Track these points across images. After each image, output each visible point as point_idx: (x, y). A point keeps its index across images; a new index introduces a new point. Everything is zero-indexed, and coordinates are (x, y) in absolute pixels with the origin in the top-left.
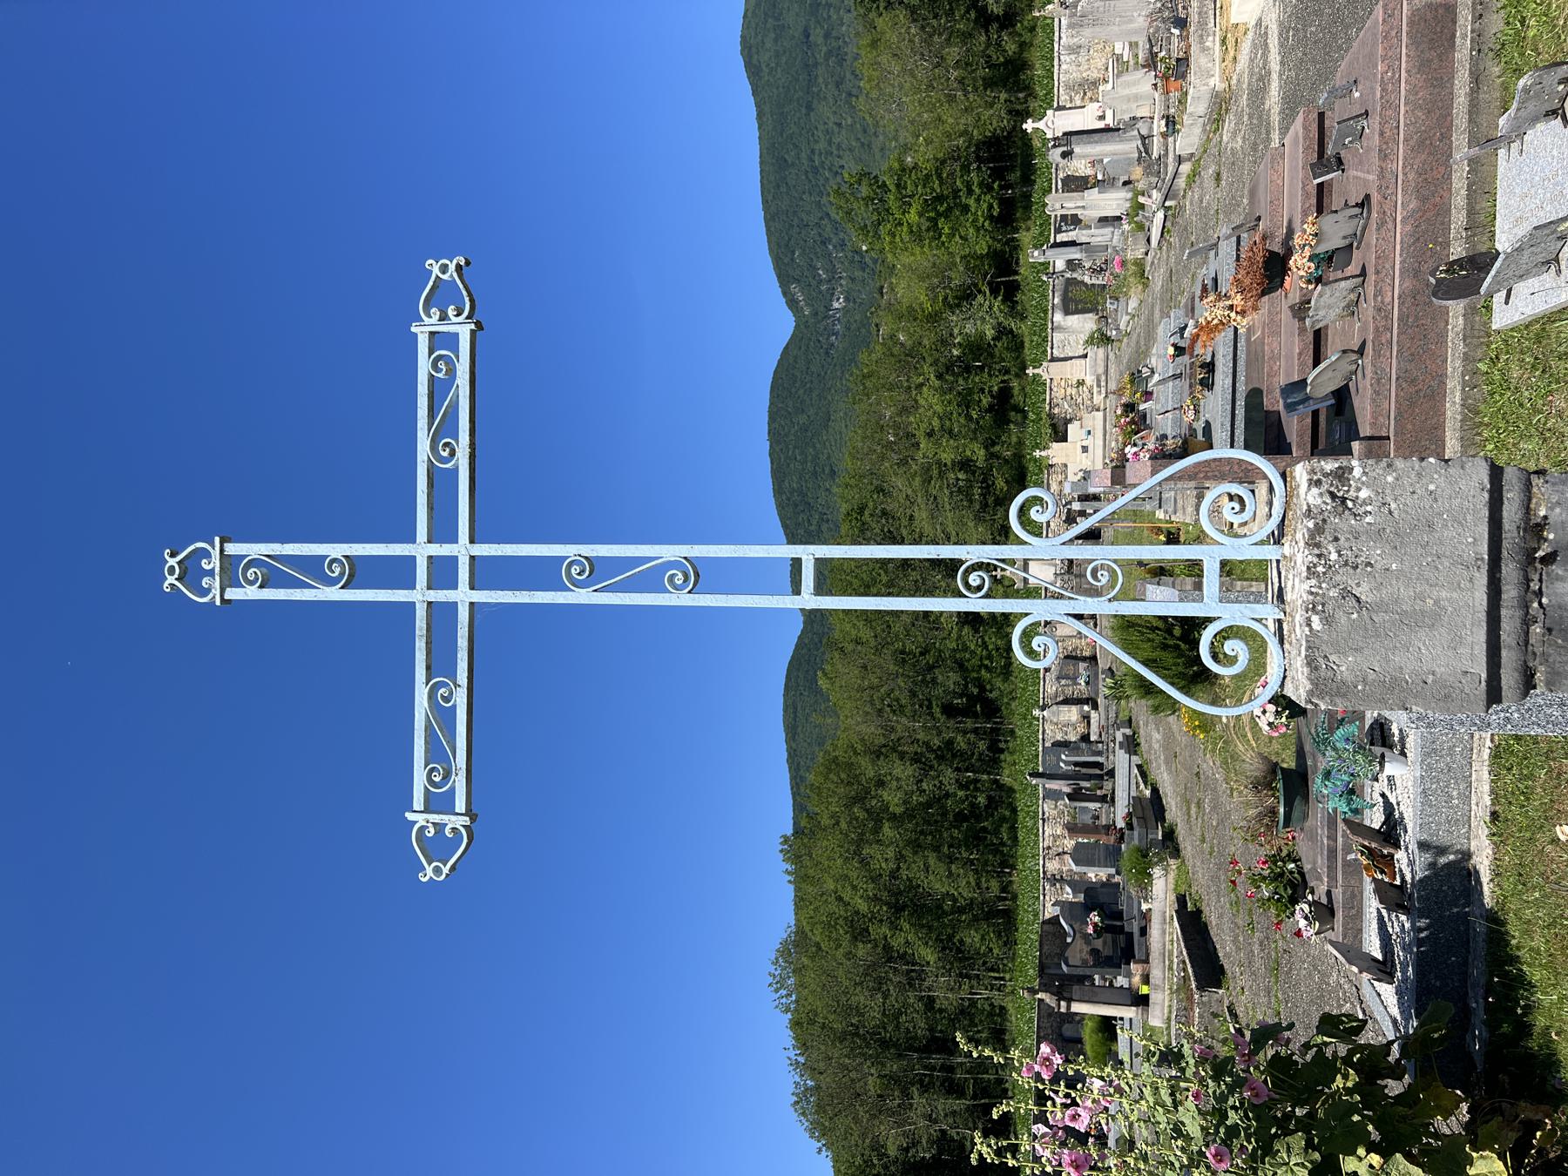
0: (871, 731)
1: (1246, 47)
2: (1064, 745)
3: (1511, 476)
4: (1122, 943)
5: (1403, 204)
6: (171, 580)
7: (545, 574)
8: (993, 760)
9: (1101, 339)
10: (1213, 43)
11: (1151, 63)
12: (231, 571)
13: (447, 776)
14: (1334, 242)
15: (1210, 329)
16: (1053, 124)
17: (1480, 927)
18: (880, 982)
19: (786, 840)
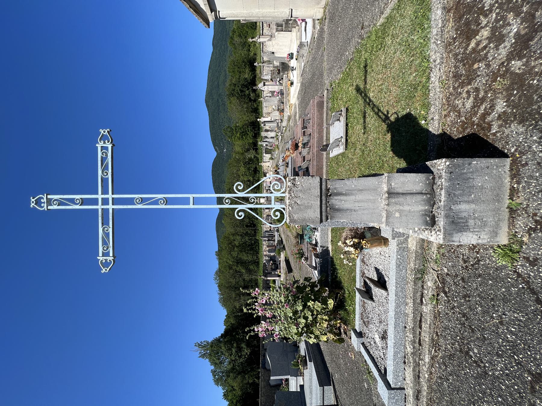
0: (232, 231)
1: (293, 108)
2: (267, 231)
3: (323, 180)
4: (276, 266)
5: (316, 135)
6: (33, 204)
7: (131, 201)
8: (255, 235)
9: (271, 159)
10: (288, 107)
11: (278, 110)
12: (49, 202)
13: (107, 248)
14: (305, 141)
15: (287, 156)
16: (262, 120)
17: (330, 260)
18: (235, 277)
19: (216, 252)
